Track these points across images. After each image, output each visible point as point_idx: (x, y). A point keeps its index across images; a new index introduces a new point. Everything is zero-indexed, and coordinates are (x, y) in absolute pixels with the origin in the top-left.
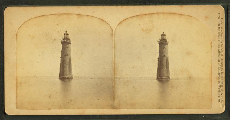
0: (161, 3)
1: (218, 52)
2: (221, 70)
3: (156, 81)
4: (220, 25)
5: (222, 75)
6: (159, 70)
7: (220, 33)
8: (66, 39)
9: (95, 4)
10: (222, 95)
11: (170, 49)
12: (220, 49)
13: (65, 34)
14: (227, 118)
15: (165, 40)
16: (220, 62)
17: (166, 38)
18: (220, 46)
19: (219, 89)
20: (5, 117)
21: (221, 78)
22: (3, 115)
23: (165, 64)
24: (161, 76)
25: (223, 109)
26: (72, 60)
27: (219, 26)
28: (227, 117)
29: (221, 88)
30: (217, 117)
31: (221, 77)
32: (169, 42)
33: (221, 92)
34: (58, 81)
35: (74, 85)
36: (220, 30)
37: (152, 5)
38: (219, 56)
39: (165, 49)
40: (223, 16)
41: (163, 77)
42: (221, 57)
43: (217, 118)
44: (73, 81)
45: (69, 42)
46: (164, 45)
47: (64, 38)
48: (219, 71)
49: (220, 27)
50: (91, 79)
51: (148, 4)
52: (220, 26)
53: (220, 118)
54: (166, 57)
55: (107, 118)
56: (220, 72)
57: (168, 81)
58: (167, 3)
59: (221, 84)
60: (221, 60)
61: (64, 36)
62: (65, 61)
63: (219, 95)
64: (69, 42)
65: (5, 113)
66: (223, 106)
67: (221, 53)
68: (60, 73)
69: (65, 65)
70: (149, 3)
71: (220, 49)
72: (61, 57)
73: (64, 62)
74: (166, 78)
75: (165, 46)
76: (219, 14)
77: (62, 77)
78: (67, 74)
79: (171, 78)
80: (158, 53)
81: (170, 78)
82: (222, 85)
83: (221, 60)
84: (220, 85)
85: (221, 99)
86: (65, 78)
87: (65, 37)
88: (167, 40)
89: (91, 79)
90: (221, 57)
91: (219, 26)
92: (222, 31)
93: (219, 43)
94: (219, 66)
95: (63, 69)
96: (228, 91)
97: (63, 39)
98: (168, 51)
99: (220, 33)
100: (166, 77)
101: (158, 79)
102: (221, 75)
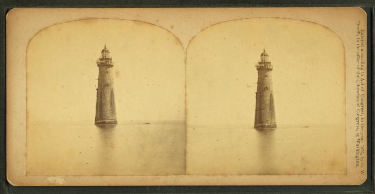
0: (263, 4)
1: (355, 85)
2: (360, 114)
3: (254, 130)
4: (360, 40)
5: (362, 123)
6: (258, 111)
7: (360, 54)
8: (264, 62)
9: (274, 5)
10: (362, 156)
11: (274, 79)
12: (360, 79)
13: (262, 54)
14: (370, 192)
15: (109, 59)
16: (360, 102)
17: (268, 59)
18: (360, 76)
19: (357, 145)
20: (7, 189)
21: (360, 127)
22: (4, 185)
23: (108, 99)
24: (261, 123)
25: (364, 177)
26: (115, 93)
27: (358, 43)
28: (369, 191)
29: (361, 144)
30: (353, 190)
31: (360, 125)
32: (274, 65)
33: (360, 151)
34: (95, 129)
35: (121, 133)
36: (360, 48)
37: (249, 7)
38: (358, 91)
39: (266, 78)
40: (364, 26)
41: (264, 124)
42: (361, 93)
43: (353, 192)
44: (117, 127)
45: (110, 63)
46: (266, 72)
47: (101, 58)
48: (358, 116)
49: (360, 44)
50: (307, 127)
51: (242, 4)
52: (360, 43)
53: (358, 191)
54: (268, 91)
55: (172, 192)
56: (360, 118)
57: (272, 130)
58: (273, 4)
59: (360, 138)
60: (360, 98)
61: (260, 57)
62: (104, 95)
63: (357, 154)
64: (110, 63)
65: (7, 183)
66: (362, 172)
67: (360, 88)
68: (256, 119)
69: (104, 101)
70: (243, 4)
71: (360, 79)
72: (97, 89)
73: (103, 97)
74: (270, 125)
75: (269, 73)
76: (358, 23)
77: (99, 121)
78: (267, 120)
79: (277, 126)
80: (97, 81)
81: (276, 125)
82: (362, 139)
83: (360, 98)
84: (358, 138)
85: (360, 162)
86: (105, 123)
87: (103, 57)
88: (270, 63)
89: (307, 127)
90: (361, 93)
91: (358, 43)
92: (362, 50)
93: (358, 70)
94: (358, 108)
95: (102, 108)
96: (372, 147)
97: (260, 63)
98: (273, 81)
99: (360, 54)
100: (110, 121)
101: (256, 127)
102: (360, 123)
